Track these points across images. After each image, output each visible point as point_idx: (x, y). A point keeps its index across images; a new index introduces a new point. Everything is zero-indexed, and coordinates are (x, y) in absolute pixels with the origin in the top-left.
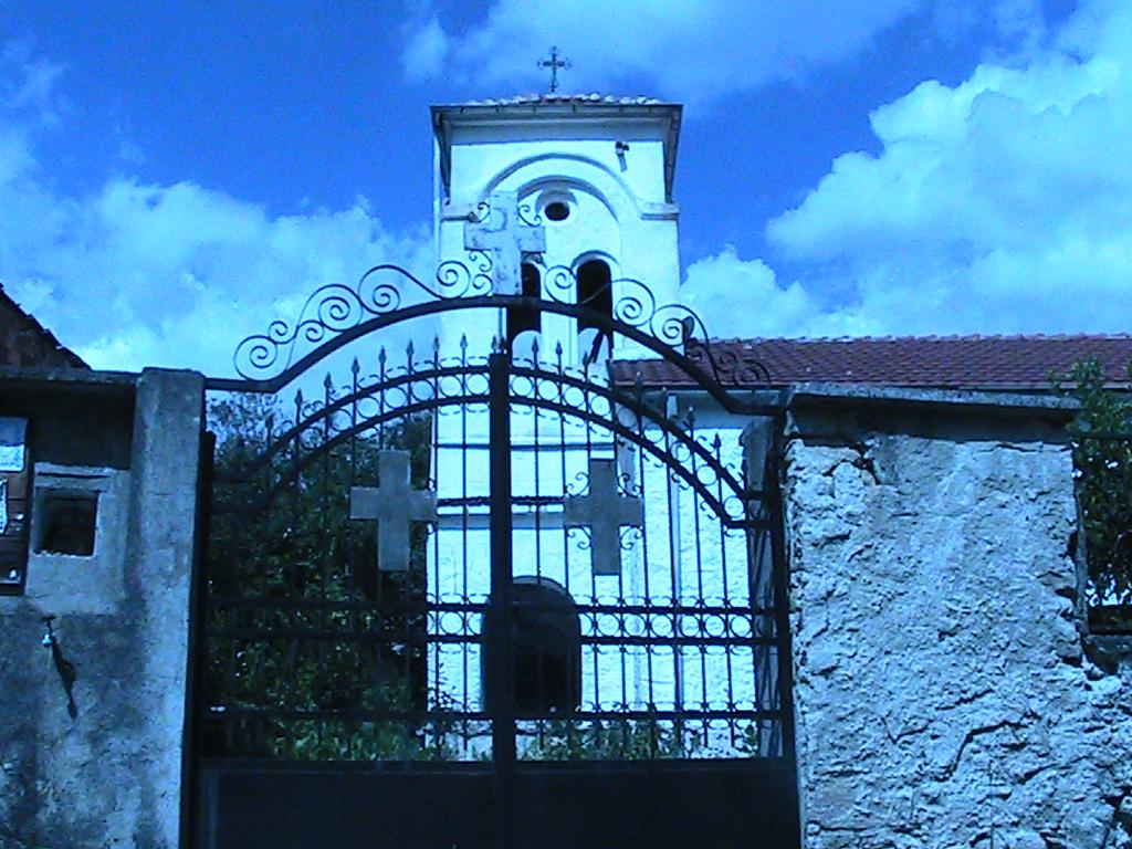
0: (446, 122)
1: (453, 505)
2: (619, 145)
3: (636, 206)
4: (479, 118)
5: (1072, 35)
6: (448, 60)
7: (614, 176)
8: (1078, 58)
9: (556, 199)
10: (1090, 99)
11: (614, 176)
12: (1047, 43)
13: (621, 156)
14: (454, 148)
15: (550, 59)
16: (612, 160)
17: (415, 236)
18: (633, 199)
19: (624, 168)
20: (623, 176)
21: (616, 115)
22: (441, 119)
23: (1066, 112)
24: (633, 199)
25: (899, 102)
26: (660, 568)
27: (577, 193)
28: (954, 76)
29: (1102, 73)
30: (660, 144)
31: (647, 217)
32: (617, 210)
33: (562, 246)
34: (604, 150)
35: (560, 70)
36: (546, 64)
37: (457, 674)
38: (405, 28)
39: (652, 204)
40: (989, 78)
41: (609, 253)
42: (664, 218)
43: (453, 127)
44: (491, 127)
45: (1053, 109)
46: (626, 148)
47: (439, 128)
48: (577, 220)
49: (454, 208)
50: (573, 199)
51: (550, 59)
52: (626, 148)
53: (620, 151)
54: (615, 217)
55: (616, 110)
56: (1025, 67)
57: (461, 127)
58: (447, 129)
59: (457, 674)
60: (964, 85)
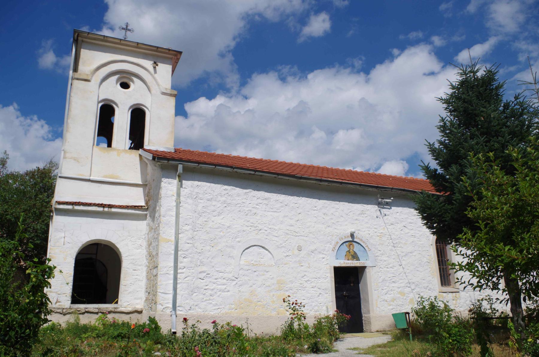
0: (79, 38)
1: (99, 207)
2: (155, 63)
3: (159, 88)
4: (95, 39)
5: (245, 91)
6: (56, 64)
7: (151, 74)
8: (246, 98)
9: (125, 80)
10: (249, 111)
11: (151, 74)
12: (238, 92)
13: (155, 68)
14: (82, 50)
15: (125, 27)
16: (151, 69)
17: (31, 119)
18: (158, 85)
19: (155, 72)
20: (156, 75)
21: (154, 51)
22: (78, 36)
23: (242, 113)
24: (158, 85)
25: (193, 102)
26: (168, 241)
27: (135, 79)
28: (211, 96)
29: (252, 103)
30: (171, 66)
31: (164, 94)
32: (152, 88)
33: (123, 102)
34: (148, 64)
35: (128, 32)
36: (123, 29)
37: (60, 289)
38: (41, 51)
39: (166, 89)
40: (220, 100)
41: (146, 105)
42: (171, 95)
43: (83, 41)
44: (101, 45)
45: (239, 112)
46: (157, 65)
47: (76, 41)
48: (134, 90)
49: (80, 74)
50: (133, 81)
51: (125, 27)
52: (157, 65)
53: (155, 65)
54: (149, 90)
55: (155, 49)
56: (231, 97)
57: (87, 42)
58: (79, 41)
59: (60, 289)
60: (213, 101)
